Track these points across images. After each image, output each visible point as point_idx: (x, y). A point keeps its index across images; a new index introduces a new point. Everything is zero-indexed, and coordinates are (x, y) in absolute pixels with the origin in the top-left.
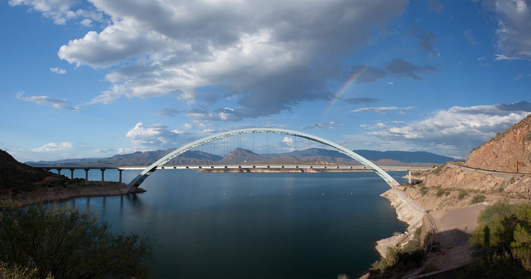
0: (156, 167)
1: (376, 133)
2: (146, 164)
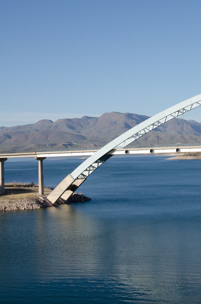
0: (113, 150)
1: (116, 301)
2: (60, 145)
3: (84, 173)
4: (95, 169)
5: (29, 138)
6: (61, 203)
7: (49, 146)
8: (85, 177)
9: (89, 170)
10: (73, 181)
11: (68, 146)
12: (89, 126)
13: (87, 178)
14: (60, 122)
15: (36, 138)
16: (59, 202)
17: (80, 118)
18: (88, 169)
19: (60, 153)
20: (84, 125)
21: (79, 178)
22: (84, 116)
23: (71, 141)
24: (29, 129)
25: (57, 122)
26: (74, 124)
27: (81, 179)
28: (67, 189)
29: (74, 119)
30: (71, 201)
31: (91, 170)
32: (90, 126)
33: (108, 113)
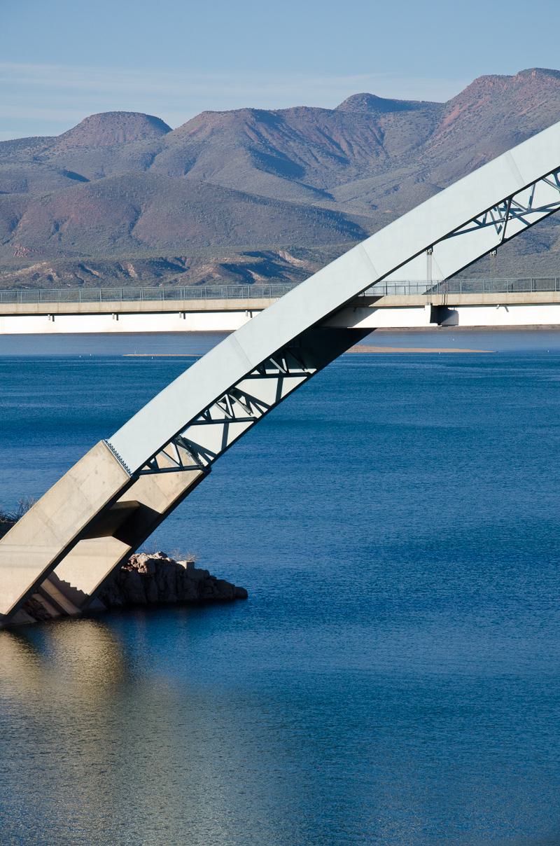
0: (360, 304)
2: (208, 269)
3: (196, 435)
4: (257, 414)
5: (21, 224)
6: (53, 613)
7: (140, 275)
8: (200, 457)
9: (226, 422)
10: (123, 480)
11: (256, 276)
12: (382, 157)
13: (214, 467)
14: (208, 129)
15: (67, 224)
16: (42, 608)
17: (333, 108)
18: (216, 413)
19: (53, 315)
20: (356, 149)
21: (162, 462)
22: (355, 98)
23: (272, 247)
24: (26, 167)
25: (191, 129)
26: (291, 143)
27: (180, 473)
28: (90, 531)
29: (297, 110)
30: (119, 602)
31: (234, 420)
32: (388, 157)
33: (500, 77)
